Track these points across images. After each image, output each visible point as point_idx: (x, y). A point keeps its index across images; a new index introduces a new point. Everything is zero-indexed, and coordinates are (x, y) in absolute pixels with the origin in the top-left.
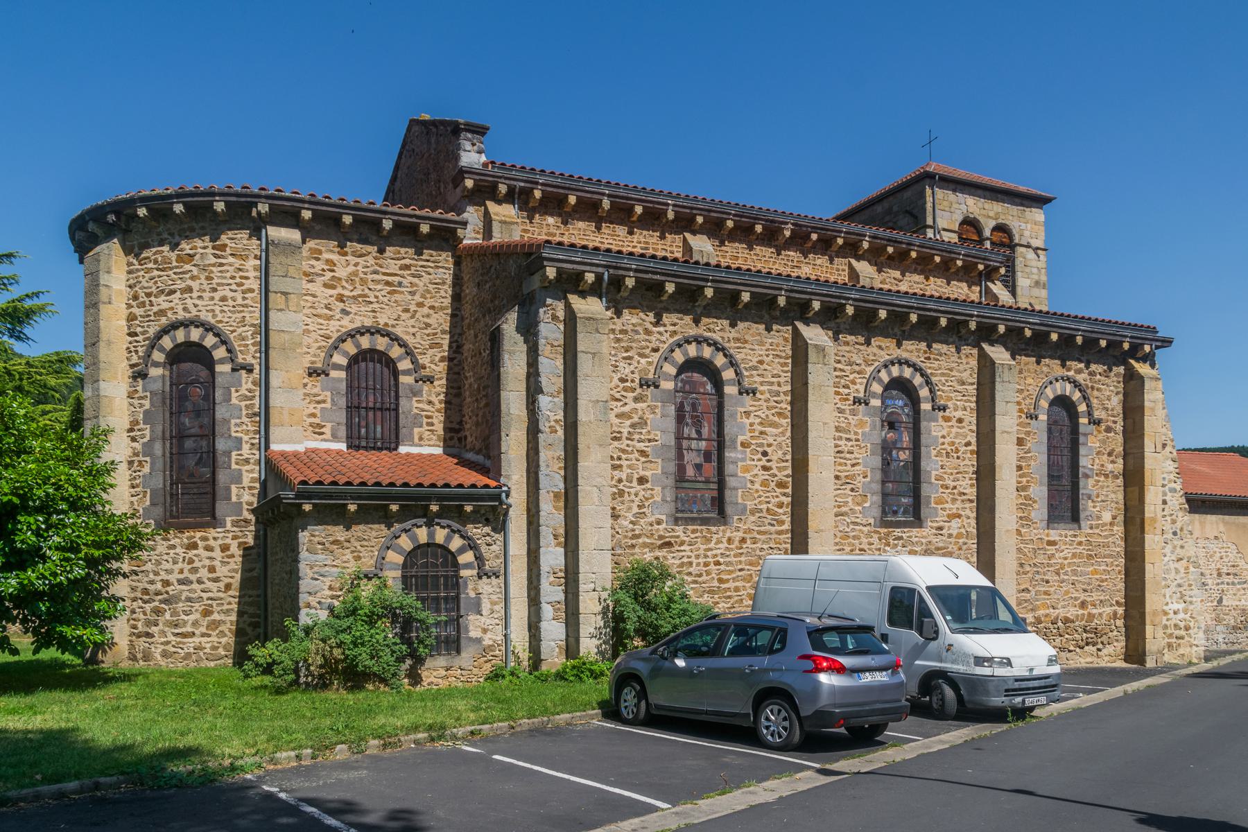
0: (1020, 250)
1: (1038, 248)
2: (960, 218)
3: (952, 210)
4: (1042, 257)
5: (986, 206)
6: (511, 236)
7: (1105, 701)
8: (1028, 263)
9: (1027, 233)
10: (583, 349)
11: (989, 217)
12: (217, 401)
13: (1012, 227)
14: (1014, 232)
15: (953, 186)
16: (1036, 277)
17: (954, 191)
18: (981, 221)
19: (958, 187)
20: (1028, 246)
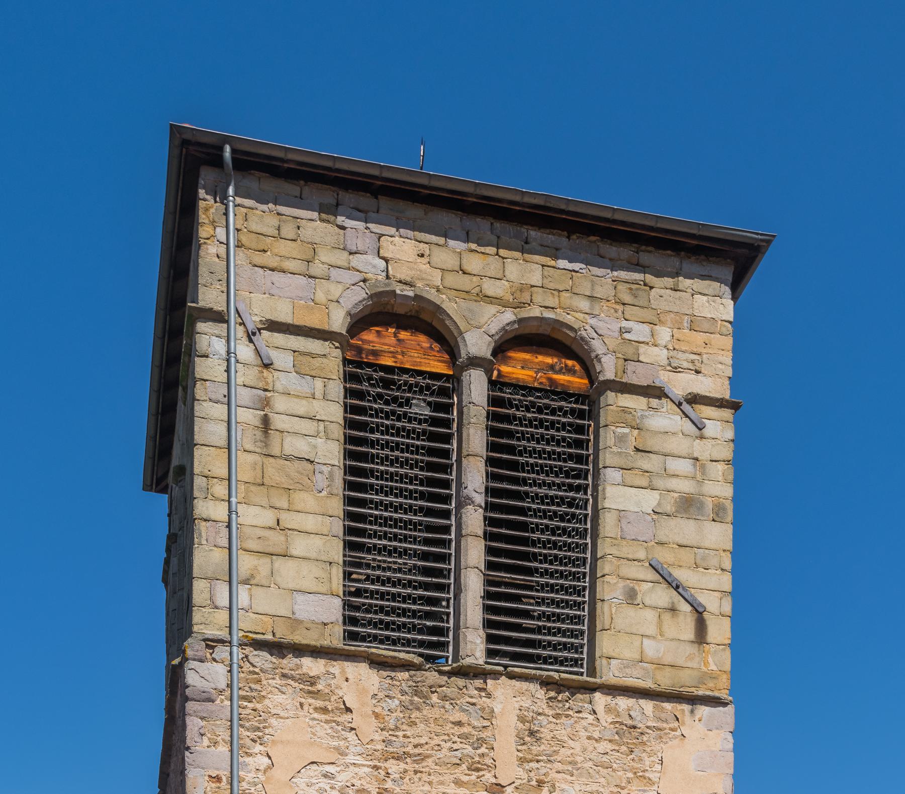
0: (614, 402)
1: (694, 399)
2: (356, 297)
3: (317, 269)
4: (713, 428)
5: (474, 263)
6: (593, 289)
7: (734, 776)
8: (652, 443)
9: (649, 354)
10: (219, 406)
11: (490, 299)
12: (430, 321)
13: (587, 333)
14: (598, 346)
15: (328, 196)
16: (686, 486)
17: (329, 210)
18: (450, 307)
19: (349, 198)
20: (654, 392)
